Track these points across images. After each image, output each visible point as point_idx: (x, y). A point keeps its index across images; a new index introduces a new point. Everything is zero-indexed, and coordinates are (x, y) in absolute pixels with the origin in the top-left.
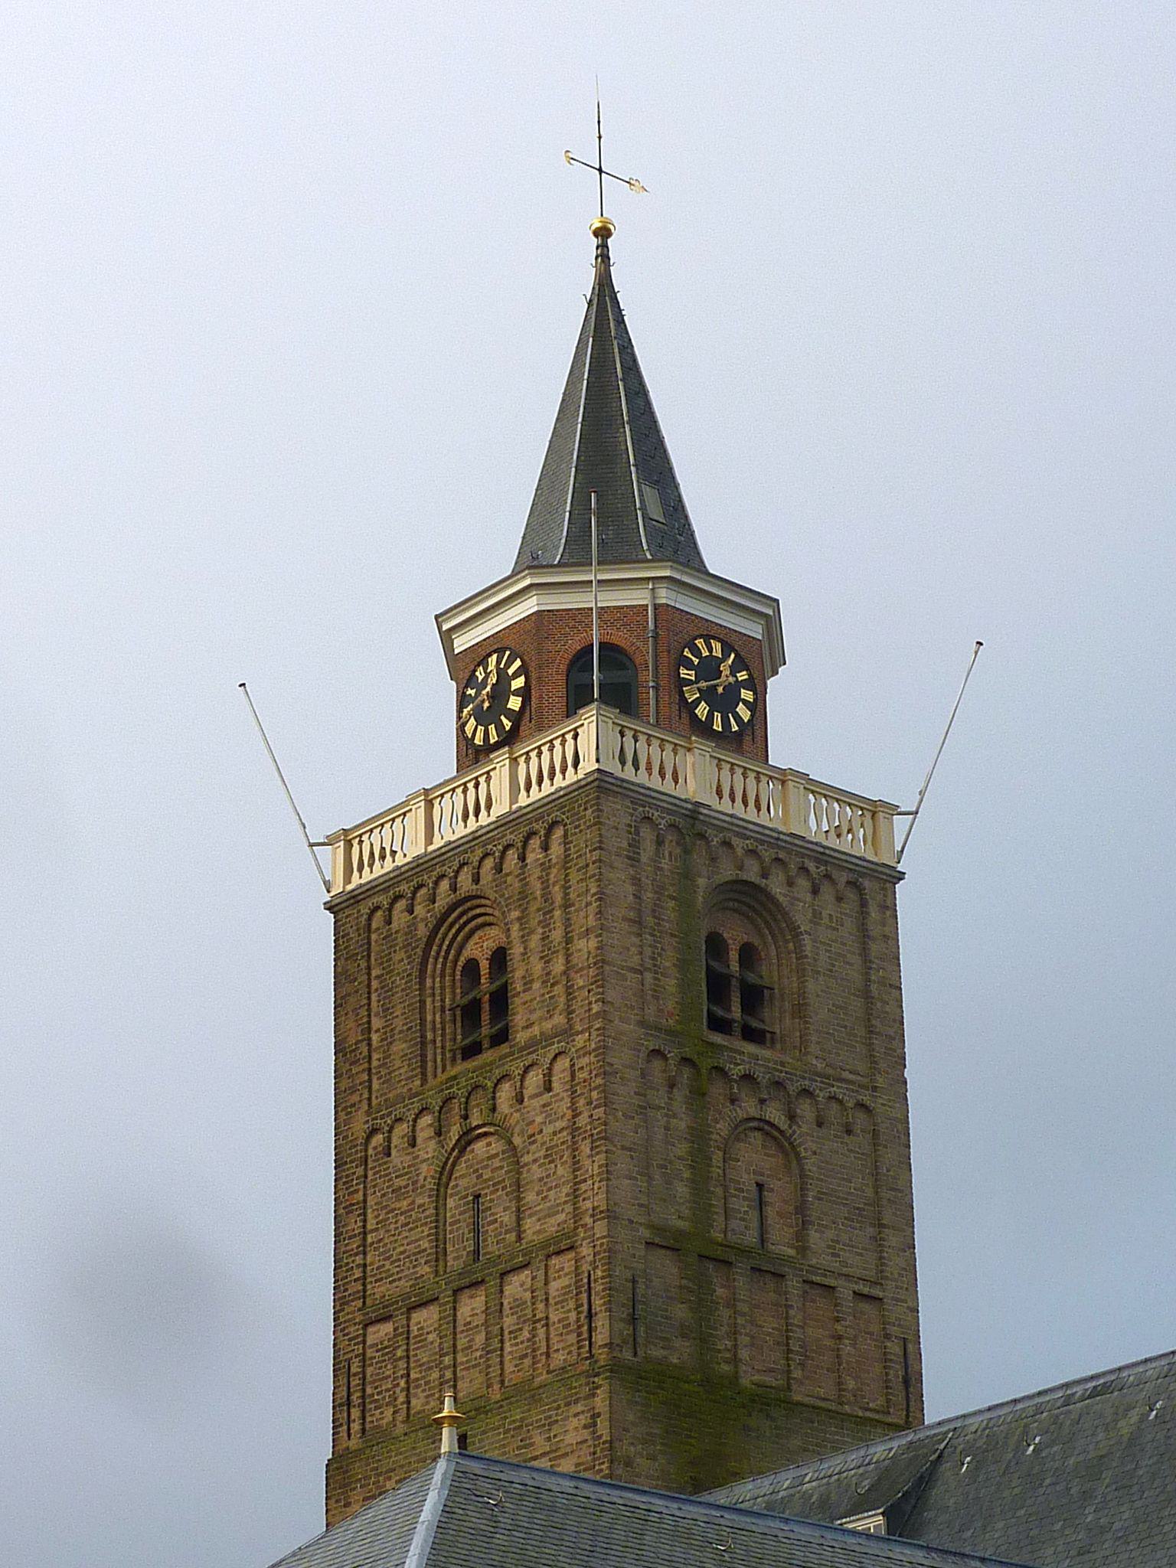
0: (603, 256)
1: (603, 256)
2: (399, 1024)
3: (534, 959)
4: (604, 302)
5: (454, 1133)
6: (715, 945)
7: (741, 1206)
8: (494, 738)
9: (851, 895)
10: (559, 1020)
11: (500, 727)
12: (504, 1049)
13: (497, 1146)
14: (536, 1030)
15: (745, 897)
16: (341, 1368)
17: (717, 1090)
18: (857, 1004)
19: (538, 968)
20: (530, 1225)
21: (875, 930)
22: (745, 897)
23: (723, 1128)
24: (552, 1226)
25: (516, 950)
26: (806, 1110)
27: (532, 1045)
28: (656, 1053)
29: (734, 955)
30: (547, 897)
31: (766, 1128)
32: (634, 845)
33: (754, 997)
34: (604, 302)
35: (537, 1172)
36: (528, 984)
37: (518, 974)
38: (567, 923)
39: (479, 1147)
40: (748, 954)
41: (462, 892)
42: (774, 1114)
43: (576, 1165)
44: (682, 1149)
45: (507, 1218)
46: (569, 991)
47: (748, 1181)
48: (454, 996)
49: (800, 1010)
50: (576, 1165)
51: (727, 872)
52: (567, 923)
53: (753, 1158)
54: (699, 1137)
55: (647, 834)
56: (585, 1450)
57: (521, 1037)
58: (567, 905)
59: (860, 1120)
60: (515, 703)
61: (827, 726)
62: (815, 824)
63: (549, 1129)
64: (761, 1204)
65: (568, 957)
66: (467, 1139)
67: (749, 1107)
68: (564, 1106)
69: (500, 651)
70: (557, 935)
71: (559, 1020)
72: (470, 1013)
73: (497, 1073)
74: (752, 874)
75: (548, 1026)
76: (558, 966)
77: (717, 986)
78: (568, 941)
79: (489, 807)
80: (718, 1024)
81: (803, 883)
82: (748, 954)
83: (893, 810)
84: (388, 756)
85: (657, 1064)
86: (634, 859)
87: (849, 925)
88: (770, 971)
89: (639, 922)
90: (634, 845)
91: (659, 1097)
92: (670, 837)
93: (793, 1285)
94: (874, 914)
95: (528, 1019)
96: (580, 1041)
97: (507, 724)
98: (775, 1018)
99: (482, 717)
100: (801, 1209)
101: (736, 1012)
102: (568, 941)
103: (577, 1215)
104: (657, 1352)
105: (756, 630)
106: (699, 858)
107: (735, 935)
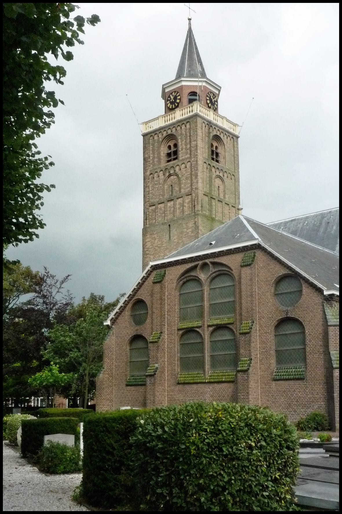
0: (190, 24)
1: (190, 24)
2: (156, 155)
3: (183, 145)
4: (190, 31)
5: (167, 174)
6: (212, 146)
7: (216, 189)
8: (174, 107)
9: (232, 139)
10: (188, 156)
11: (175, 105)
12: (176, 161)
13: (175, 177)
14: (184, 157)
15: (217, 138)
16: (145, 213)
17: (213, 170)
18: (233, 158)
19: (184, 147)
20: (182, 190)
21: (235, 146)
22: (217, 138)
23: (214, 176)
24: (187, 190)
25: (180, 144)
26: (226, 175)
27: (183, 160)
28: (205, 162)
29: (214, 148)
30: (186, 135)
31: (219, 177)
32: (202, 126)
33: (217, 155)
34: (190, 31)
35: (184, 181)
36: (182, 149)
37: (180, 148)
38: (190, 139)
39: (172, 177)
40: (216, 147)
41: (169, 133)
42: (221, 175)
43: (192, 180)
44: (208, 179)
45: (177, 189)
46: (191, 151)
47: (217, 186)
48: (166, 151)
49: (225, 158)
50: (192, 180)
51: (215, 133)
52: (190, 139)
53: (218, 182)
54: (210, 178)
55: (204, 125)
56: (193, 228)
57: (181, 159)
58: (190, 136)
59: (233, 177)
60: (178, 101)
61: (230, 110)
62: (226, 126)
63: (186, 174)
64: (219, 190)
65: (190, 145)
66: (170, 175)
67: (218, 173)
68: (189, 170)
69: (175, 92)
70: (188, 141)
71: (188, 156)
72: (169, 155)
73: (176, 164)
74: (218, 134)
75: (186, 157)
76: (188, 146)
77: (213, 151)
78: (190, 142)
79: (192, 111)
80: (213, 159)
81: (225, 136)
82: (216, 147)
83: (238, 125)
84: (153, 111)
85: (205, 164)
86: (202, 129)
87: (232, 145)
88: (219, 151)
89: (202, 140)
90: (202, 126)
91: (205, 170)
92: (207, 126)
93: (224, 203)
94: (235, 143)
95: (181, 155)
96: (193, 159)
97: (177, 105)
98: (221, 159)
99: (172, 103)
100: (224, 191)
101: (215, 157)
102: (190, 142)
103: (192, 189)
104: (205, 212)
105: (217, 92)
106: (211, 130)
107: (215, 144)
